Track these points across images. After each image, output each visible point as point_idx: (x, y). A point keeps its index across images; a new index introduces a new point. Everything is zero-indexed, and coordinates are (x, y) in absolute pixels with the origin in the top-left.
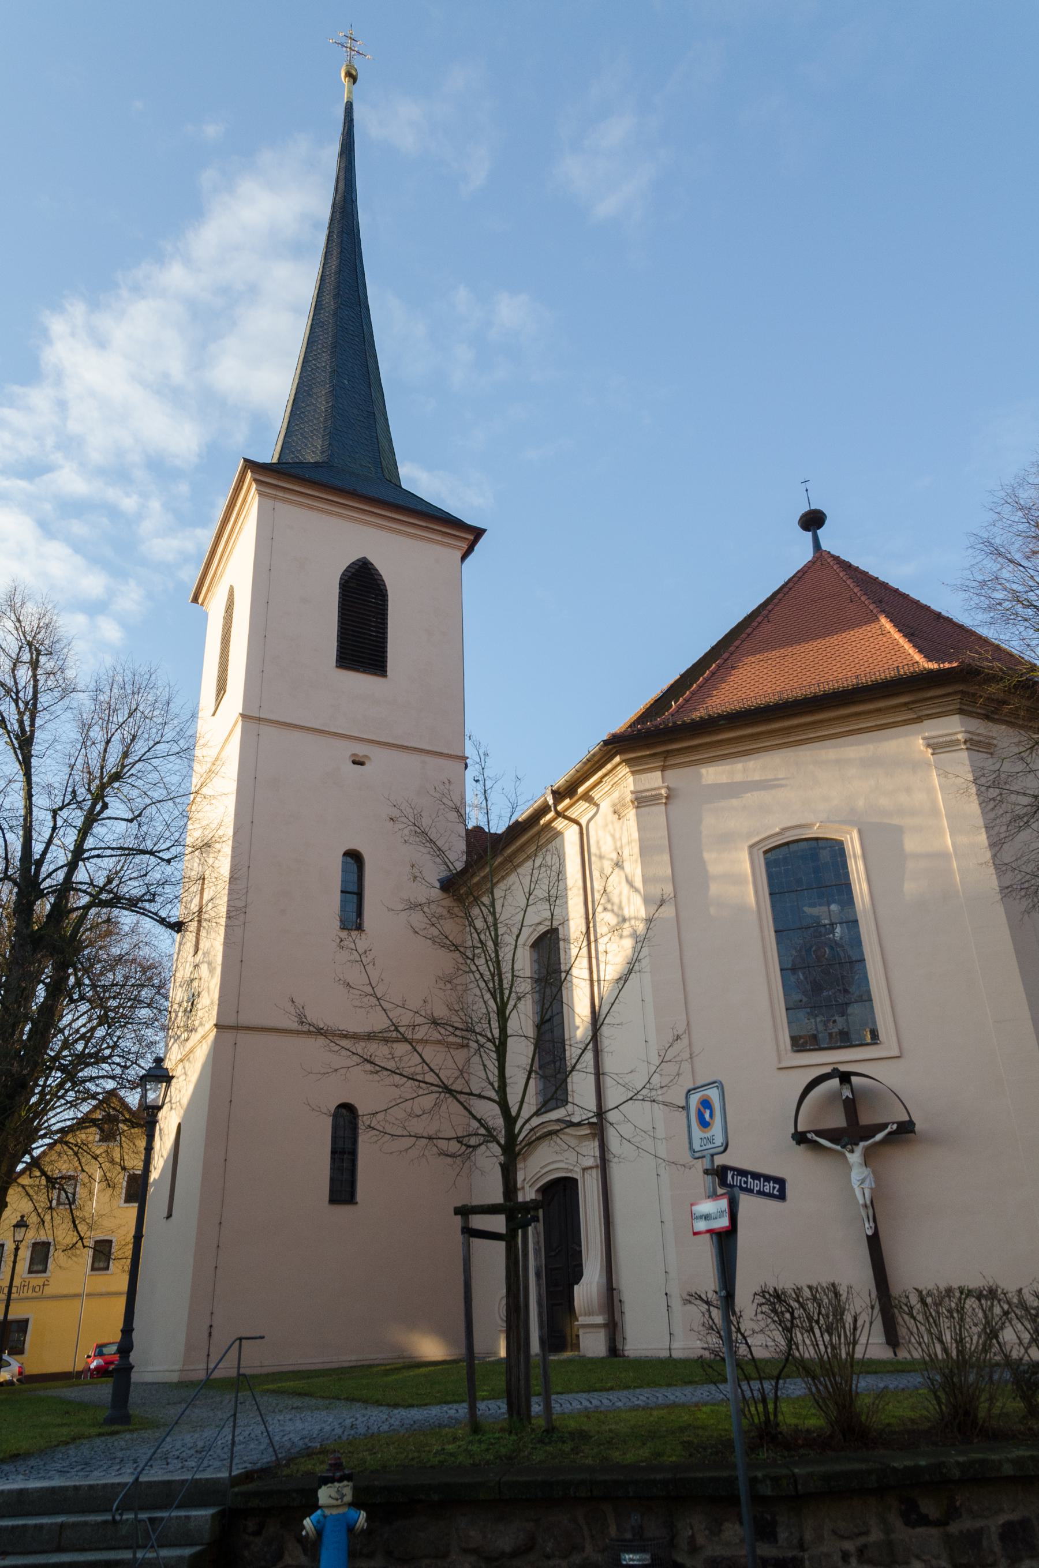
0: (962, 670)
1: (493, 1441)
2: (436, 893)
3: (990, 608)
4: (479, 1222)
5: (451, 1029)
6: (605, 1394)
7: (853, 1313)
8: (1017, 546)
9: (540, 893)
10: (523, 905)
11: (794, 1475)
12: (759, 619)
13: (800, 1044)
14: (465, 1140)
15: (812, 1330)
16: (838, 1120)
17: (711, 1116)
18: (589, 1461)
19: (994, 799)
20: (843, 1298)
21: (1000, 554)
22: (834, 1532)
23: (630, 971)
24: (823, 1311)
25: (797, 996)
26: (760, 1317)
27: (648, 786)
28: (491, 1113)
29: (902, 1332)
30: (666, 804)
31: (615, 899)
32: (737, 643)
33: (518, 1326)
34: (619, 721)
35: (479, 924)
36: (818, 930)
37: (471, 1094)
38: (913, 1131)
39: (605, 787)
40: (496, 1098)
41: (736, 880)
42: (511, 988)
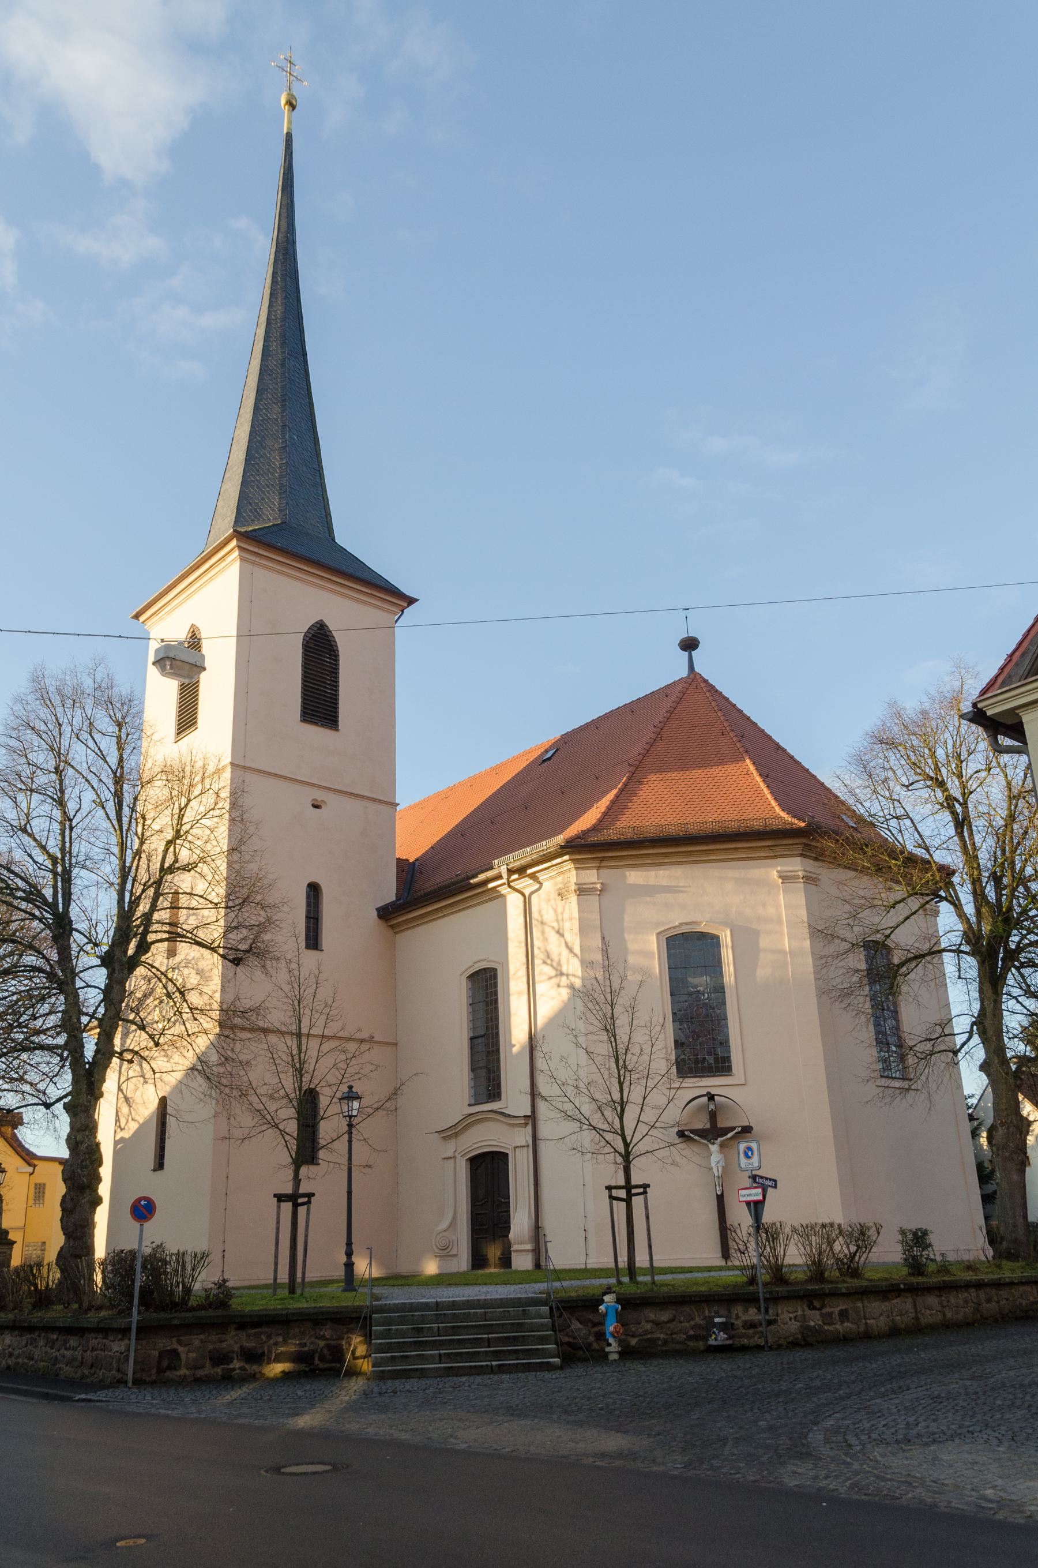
4: (615, 1193)
17: (752, 1154)
31: (555, 958)
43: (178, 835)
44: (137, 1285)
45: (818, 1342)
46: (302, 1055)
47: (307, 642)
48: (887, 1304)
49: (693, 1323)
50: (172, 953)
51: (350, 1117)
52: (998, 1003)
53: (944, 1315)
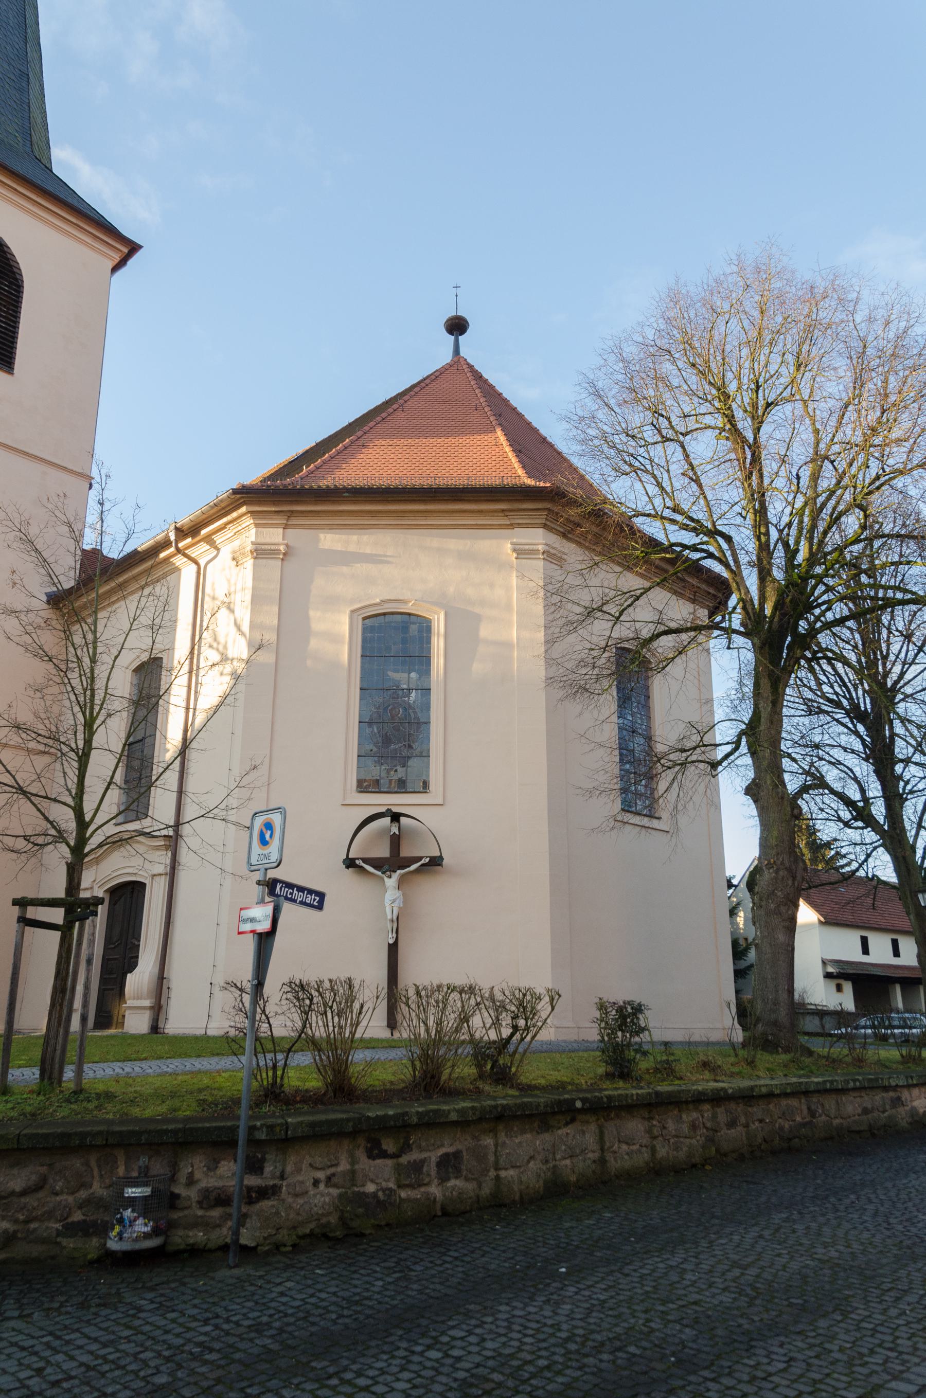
0: (552, 491)
1: (19, 1101)
2: (39, 603)
3: (583, 442)
4: (33, 913)
5: (34, 735)
6: (138, 1063)
7: (361, 1001)
8: (613, 392)
9: (144, 620)
10: (126, 628)
11: (287, 1123)
12: (395, 406)
13: (363, 786)
14: (32, 839)
15: (325, 1013)
16: (383, 851)
17: (271, 836)
18: (111, 1116)
19: (555, 604)
20: (356, 989)
21: (600, 397)
22: (311, 1165)
23: (221, 704)
24: (338, 999)
25: (369, 747)
26: (284, 1002)
27: (268, 540)
28: (66, 818)
29: (399, 1017)
30: (282, 559)
31: (222, 639)
32: (372, 424)
33: (61, 1005)
34: (252, 476)
35: (78, 639)
36: (396, 692)
37: (47, 797)
38: (440, 865)
39: (228, 533)
40: (72, 804)
41: (334, 638)
42: (102, 704)
45: (379, 1227)
48: (546, 1136)
49: (83, 1194)
52: (777, 702)
53: (653, 1150)
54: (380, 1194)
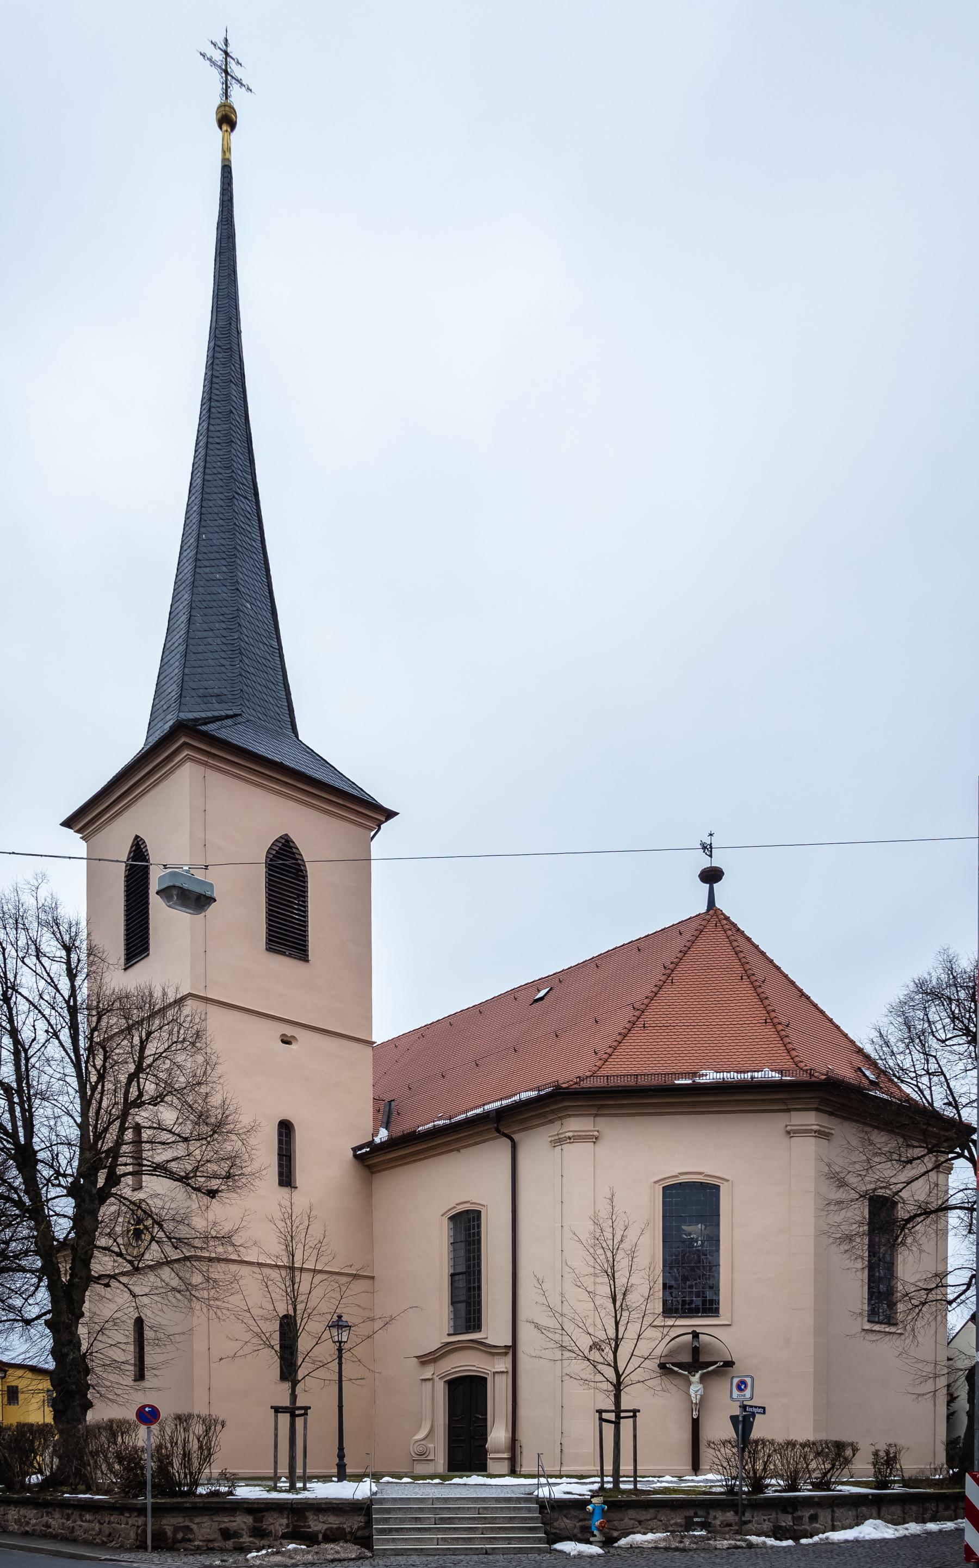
4: (605, 1416)
13: (669, 1311)
16: (686, 1358)
17: (746, 1387)
43: (139, 1069)
44: (148, 1474)
46: (296, 1286)
47: (271, 860)
50: (138, 1187)
51: (340, 1342)
54: (787, 1527)
